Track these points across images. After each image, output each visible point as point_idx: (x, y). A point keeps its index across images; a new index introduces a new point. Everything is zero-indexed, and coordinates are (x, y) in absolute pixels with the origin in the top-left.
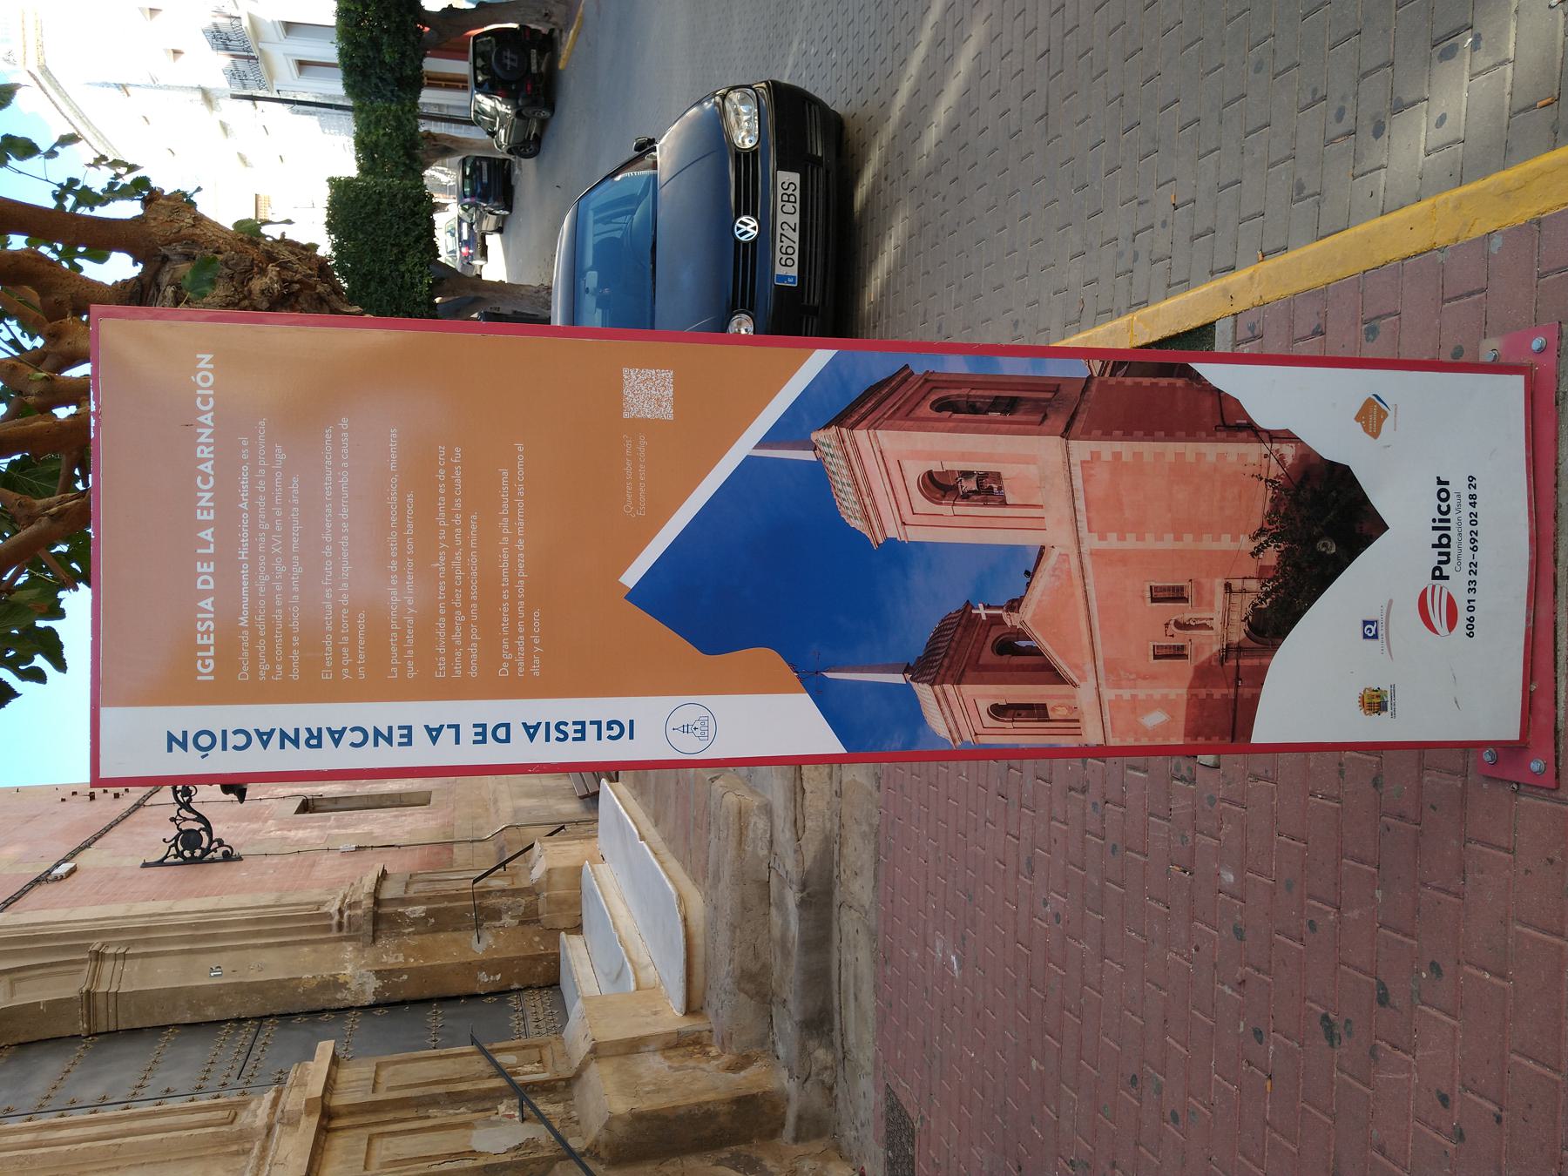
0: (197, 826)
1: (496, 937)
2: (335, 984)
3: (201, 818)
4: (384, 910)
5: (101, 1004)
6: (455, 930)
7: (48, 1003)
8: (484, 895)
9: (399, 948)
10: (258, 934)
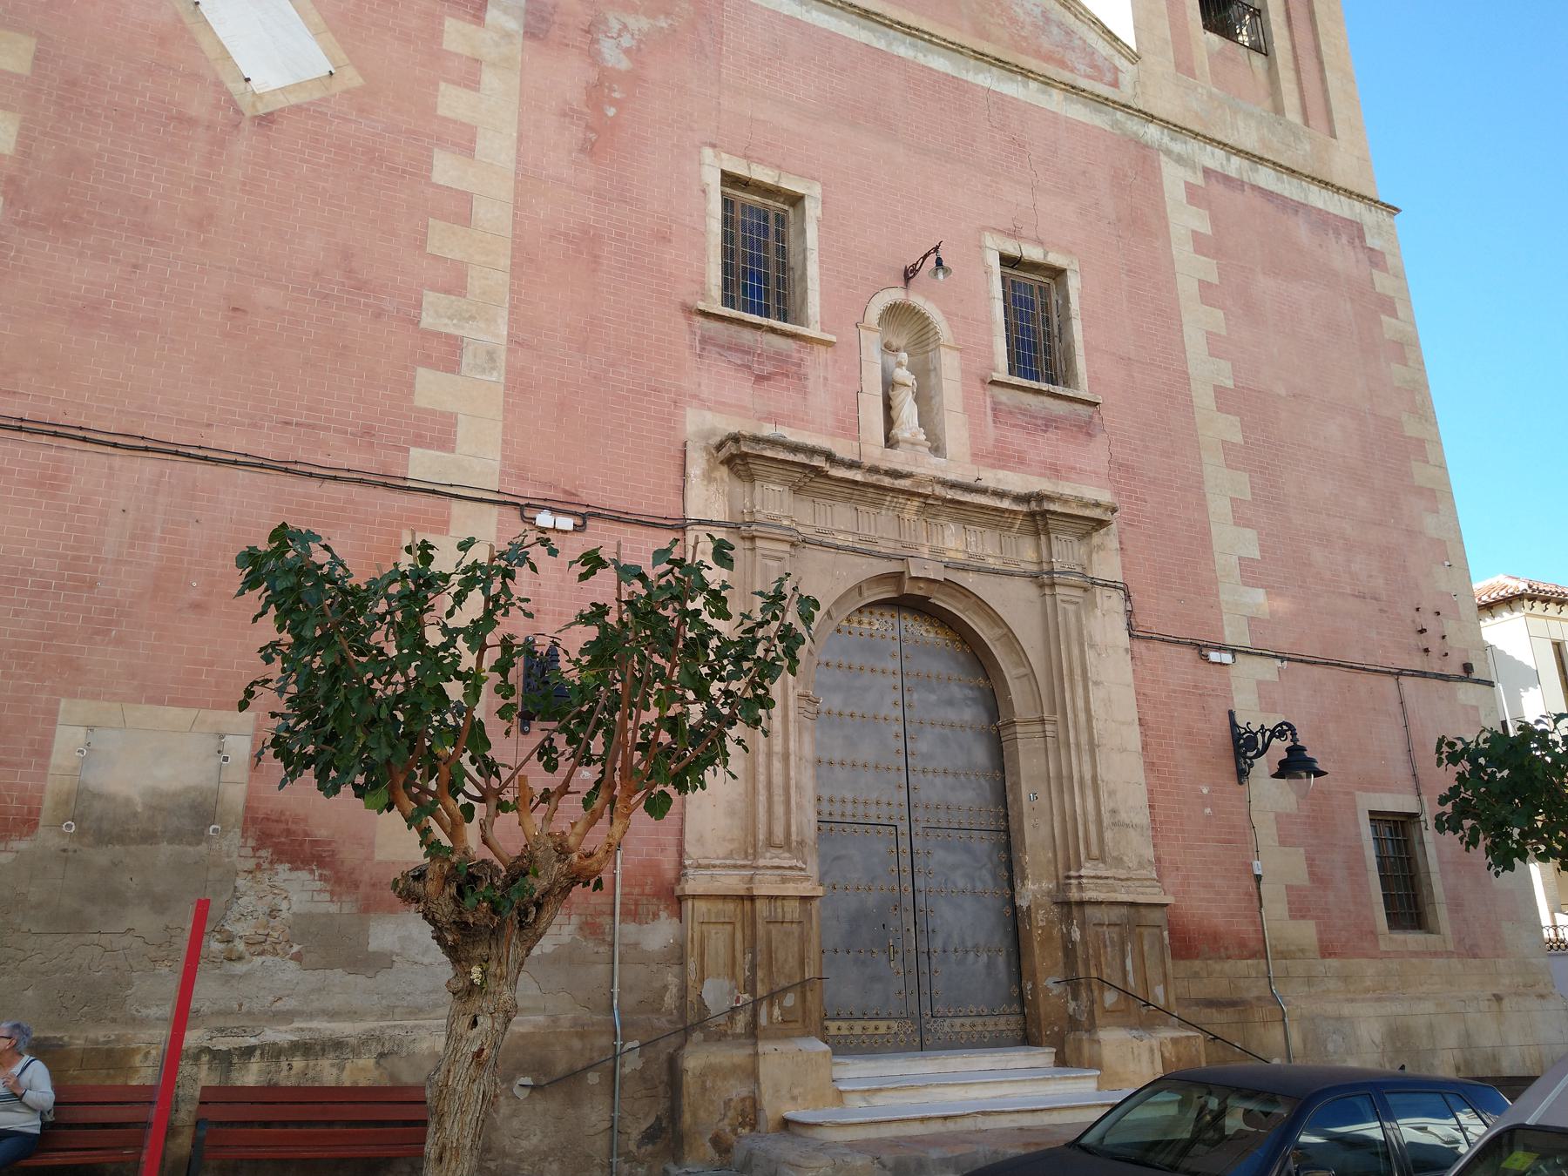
0: (1260, 746)
1: (1059, 996)
2: (1024, 878)
3: (1266, 746)
4: (1075, 911)
5: (1011, 731)
6: (1065, 964)
7: (1011, 699)
8: (1089, 986)
9: (1050, 922)
10: (1064, 821)
